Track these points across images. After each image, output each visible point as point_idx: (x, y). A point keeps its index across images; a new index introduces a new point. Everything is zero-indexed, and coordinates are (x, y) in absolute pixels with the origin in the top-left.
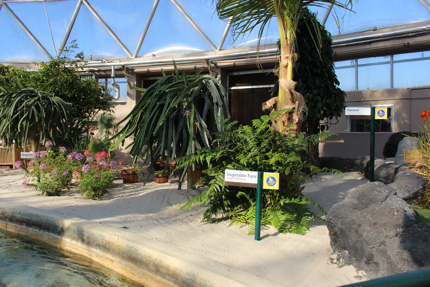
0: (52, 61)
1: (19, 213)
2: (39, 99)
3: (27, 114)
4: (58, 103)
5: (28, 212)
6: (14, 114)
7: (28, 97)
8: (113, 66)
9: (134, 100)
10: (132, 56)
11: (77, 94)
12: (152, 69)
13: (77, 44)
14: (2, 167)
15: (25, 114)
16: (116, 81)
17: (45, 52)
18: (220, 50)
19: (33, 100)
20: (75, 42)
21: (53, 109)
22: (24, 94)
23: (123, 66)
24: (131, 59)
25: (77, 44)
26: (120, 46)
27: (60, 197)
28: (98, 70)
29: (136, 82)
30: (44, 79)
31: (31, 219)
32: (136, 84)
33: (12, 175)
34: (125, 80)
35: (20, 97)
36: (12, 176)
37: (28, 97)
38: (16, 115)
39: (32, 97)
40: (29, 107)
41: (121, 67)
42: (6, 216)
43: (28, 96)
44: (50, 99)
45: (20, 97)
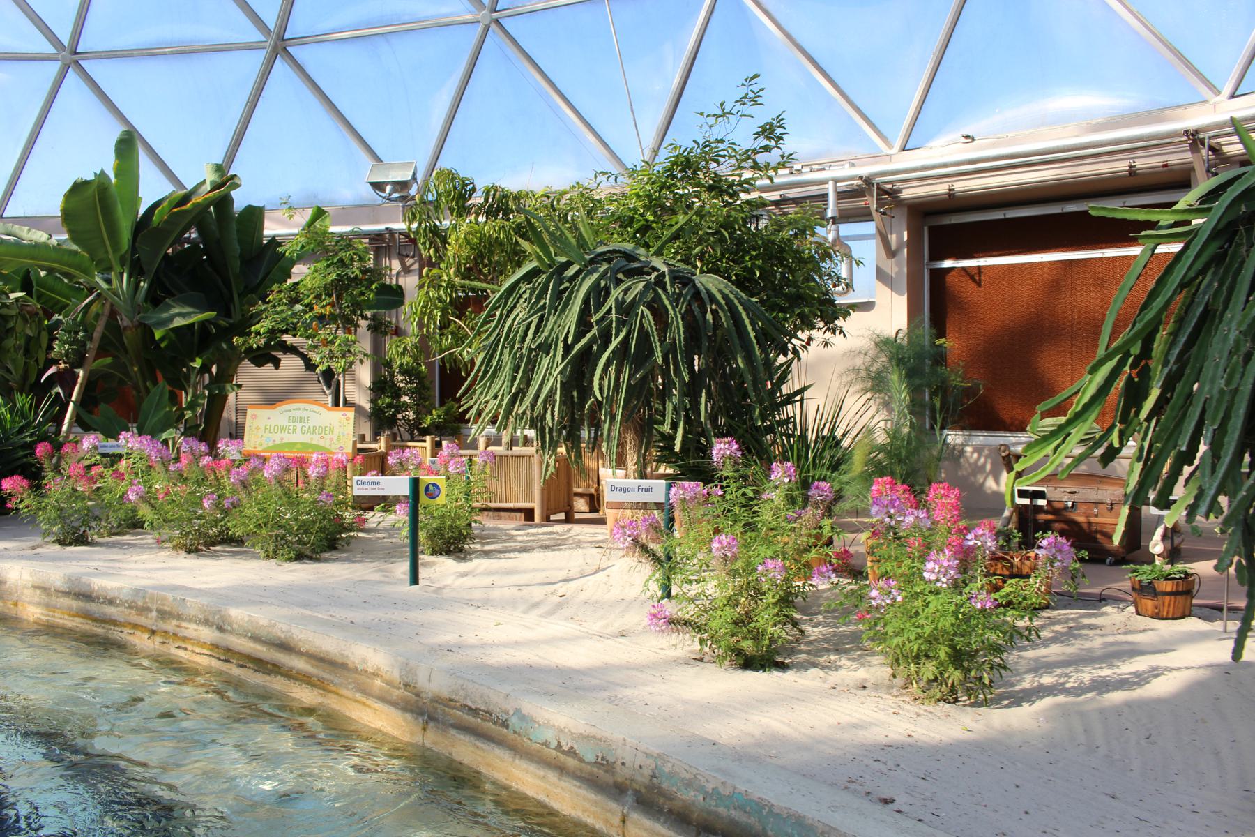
0: (677, 157)
1: (689, 784)
2: (660, 282)
3: (622, 335)
4: (725, 297)
5: (741, 787)
6: (579, 335)
7: (620, 276)
8: (831, 183)
9: (901, 294)
10: (890, 146)
11: (760, 268)
12: (964, 186)
13: (762, 90)
14: (503, 514)
15: (617, 336)
16: (841, 234)
17: (608, 155)
18: (1233, 96)
19: (641, 286)
20: (752, 82)
21: (709, 316)
22: (605, 266)
23: (868, 181)
24: (888, 158)
25: (762, 90)
26: (851, 118)
27: (790, 676)
28: (778, 198)
29: (905, 233)
30: (647, 221)
31: (758, 827)
32: (906, 238)
33: (546, 547)
34: (869, 228)
35: (596, 275)
36: (549, 554)
37: (620, 276)
38: (584, 341)
39: (639, 272)
40: (627, 310)
41: (860, 182)
42: (619, 779)
43: (618, 271)
44: (697, 282)
45: (596, 275)
